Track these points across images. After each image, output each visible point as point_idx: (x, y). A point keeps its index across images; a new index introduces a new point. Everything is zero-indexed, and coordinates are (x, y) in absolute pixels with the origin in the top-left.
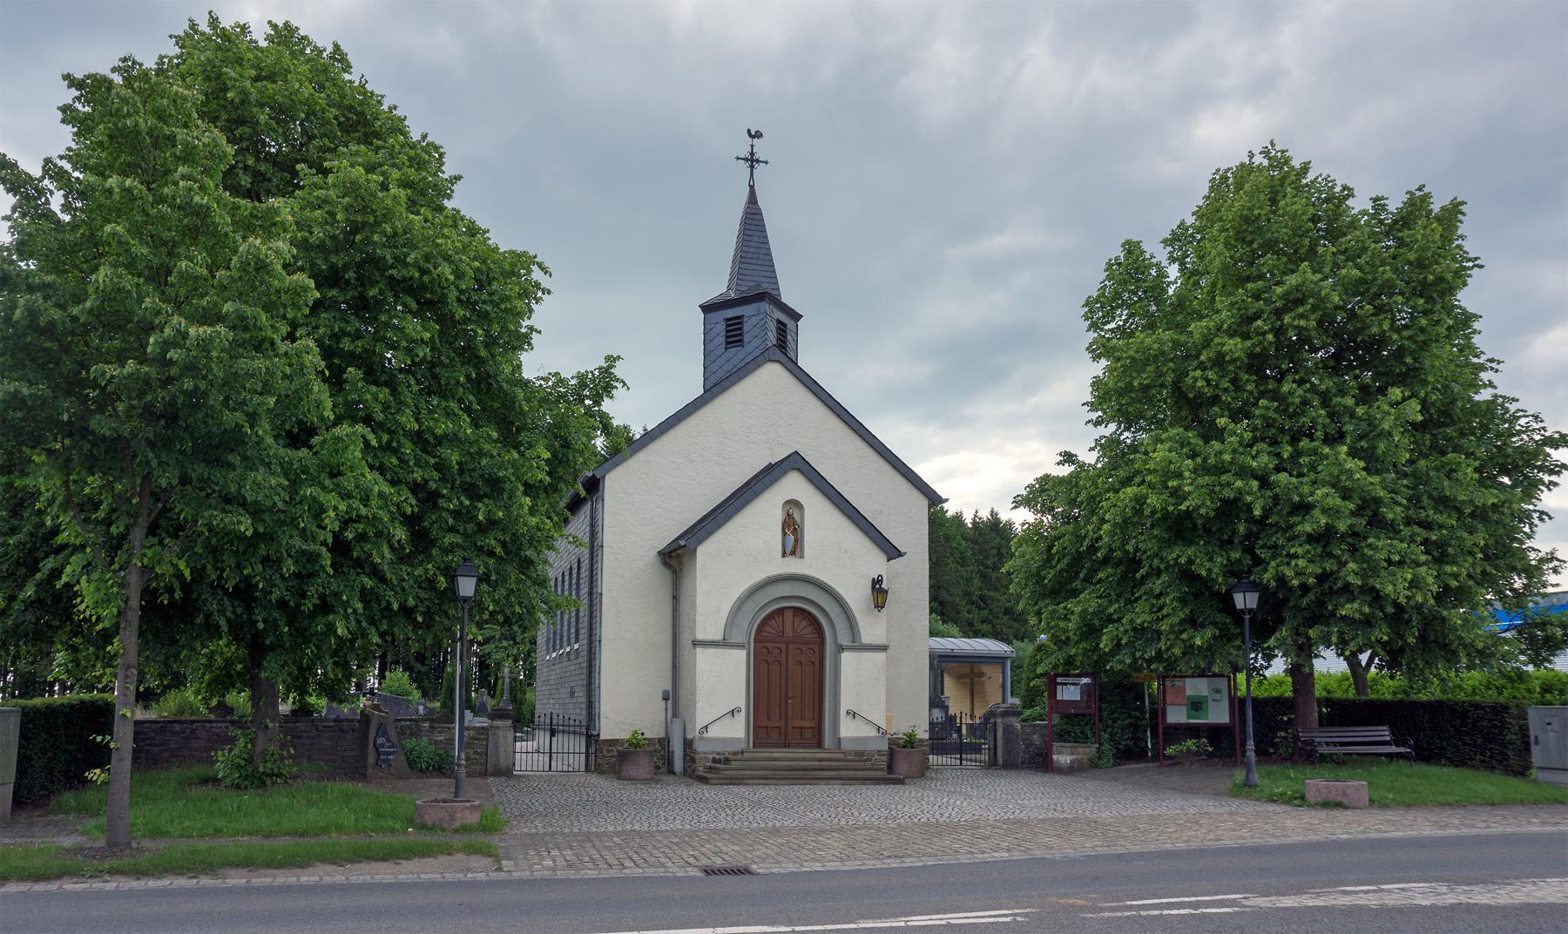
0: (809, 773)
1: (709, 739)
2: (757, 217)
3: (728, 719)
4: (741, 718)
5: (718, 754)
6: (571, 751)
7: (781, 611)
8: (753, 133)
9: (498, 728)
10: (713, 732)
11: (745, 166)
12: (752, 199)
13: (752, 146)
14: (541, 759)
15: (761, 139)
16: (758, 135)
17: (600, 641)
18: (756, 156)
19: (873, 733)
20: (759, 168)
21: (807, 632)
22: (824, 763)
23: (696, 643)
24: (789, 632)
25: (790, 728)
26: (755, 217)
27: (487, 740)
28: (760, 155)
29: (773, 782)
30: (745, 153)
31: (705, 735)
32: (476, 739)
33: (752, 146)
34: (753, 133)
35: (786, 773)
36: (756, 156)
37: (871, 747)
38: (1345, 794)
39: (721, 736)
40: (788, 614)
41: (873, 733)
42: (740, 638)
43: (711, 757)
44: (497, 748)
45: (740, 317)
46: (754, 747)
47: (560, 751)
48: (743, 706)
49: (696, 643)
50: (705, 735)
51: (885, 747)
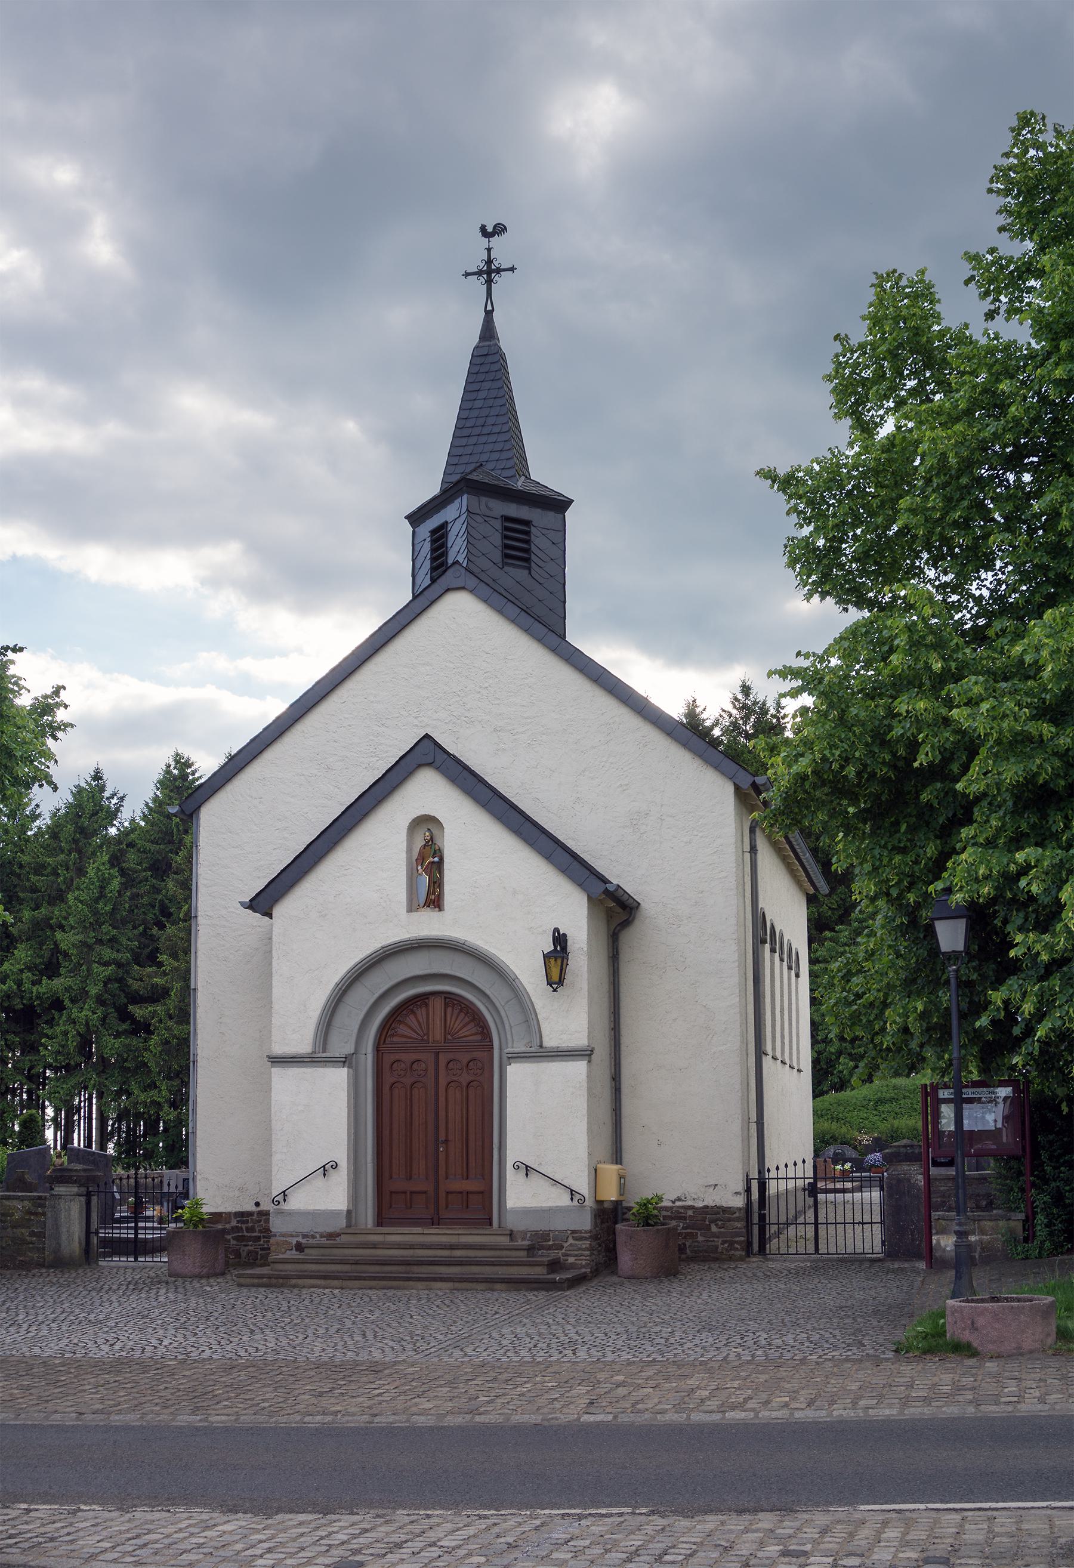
0: (415, 1269)
1: (291, 1213)
2: (496, 358)
3: (319, 1181)
4: (340, 1180)
5: (305, 1236)
6: (840, 1227)
7: (422, 999)
8: (490, 229)
9: (59, 1196)
10: (297, 1202)
11: (477, 285)
12: (488, 331)
13: (489, 250)
14: (868, 1234)
15: (504, 237)
16: (500, 229)
17: (194, 1062)
18: (496, 264)
19: (563, 1200)
20: (501, 282)
21: (468, 1032)
22: (458, 1253)
23: (585, 1054)
24: (437, 1033)
25: (442, 1195)
26: (490, 359)
27: (44, 1214)
28: (501, 260)
29: (336, 1283)
30: (477, 262)
31: (285, 1207)
32: (32, 1214)
33: (489, 250)
34: (490, 229)
35: (377, 1268)
36: (496, 264)
37: (560, 1224)
38: (974, 1327)
39: (311, 1208)
40: (437, 1004)
41: (563, 1200)
42: (342, 1044)
43: (294, 1241)
44: (57, 1226)
45: (528, 523)
46: (380, 1221)
47: (840, 1219)
48: (342, 1156)
49: (585, 1054)
50: (285, 1207)
51: (585, 1222)
